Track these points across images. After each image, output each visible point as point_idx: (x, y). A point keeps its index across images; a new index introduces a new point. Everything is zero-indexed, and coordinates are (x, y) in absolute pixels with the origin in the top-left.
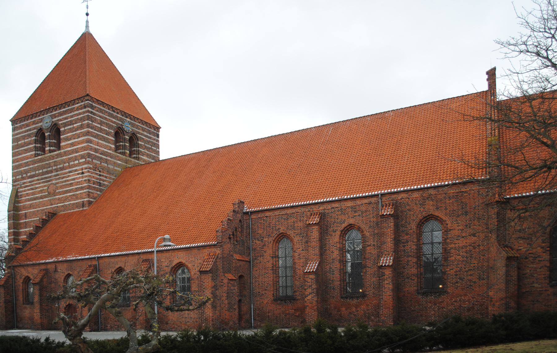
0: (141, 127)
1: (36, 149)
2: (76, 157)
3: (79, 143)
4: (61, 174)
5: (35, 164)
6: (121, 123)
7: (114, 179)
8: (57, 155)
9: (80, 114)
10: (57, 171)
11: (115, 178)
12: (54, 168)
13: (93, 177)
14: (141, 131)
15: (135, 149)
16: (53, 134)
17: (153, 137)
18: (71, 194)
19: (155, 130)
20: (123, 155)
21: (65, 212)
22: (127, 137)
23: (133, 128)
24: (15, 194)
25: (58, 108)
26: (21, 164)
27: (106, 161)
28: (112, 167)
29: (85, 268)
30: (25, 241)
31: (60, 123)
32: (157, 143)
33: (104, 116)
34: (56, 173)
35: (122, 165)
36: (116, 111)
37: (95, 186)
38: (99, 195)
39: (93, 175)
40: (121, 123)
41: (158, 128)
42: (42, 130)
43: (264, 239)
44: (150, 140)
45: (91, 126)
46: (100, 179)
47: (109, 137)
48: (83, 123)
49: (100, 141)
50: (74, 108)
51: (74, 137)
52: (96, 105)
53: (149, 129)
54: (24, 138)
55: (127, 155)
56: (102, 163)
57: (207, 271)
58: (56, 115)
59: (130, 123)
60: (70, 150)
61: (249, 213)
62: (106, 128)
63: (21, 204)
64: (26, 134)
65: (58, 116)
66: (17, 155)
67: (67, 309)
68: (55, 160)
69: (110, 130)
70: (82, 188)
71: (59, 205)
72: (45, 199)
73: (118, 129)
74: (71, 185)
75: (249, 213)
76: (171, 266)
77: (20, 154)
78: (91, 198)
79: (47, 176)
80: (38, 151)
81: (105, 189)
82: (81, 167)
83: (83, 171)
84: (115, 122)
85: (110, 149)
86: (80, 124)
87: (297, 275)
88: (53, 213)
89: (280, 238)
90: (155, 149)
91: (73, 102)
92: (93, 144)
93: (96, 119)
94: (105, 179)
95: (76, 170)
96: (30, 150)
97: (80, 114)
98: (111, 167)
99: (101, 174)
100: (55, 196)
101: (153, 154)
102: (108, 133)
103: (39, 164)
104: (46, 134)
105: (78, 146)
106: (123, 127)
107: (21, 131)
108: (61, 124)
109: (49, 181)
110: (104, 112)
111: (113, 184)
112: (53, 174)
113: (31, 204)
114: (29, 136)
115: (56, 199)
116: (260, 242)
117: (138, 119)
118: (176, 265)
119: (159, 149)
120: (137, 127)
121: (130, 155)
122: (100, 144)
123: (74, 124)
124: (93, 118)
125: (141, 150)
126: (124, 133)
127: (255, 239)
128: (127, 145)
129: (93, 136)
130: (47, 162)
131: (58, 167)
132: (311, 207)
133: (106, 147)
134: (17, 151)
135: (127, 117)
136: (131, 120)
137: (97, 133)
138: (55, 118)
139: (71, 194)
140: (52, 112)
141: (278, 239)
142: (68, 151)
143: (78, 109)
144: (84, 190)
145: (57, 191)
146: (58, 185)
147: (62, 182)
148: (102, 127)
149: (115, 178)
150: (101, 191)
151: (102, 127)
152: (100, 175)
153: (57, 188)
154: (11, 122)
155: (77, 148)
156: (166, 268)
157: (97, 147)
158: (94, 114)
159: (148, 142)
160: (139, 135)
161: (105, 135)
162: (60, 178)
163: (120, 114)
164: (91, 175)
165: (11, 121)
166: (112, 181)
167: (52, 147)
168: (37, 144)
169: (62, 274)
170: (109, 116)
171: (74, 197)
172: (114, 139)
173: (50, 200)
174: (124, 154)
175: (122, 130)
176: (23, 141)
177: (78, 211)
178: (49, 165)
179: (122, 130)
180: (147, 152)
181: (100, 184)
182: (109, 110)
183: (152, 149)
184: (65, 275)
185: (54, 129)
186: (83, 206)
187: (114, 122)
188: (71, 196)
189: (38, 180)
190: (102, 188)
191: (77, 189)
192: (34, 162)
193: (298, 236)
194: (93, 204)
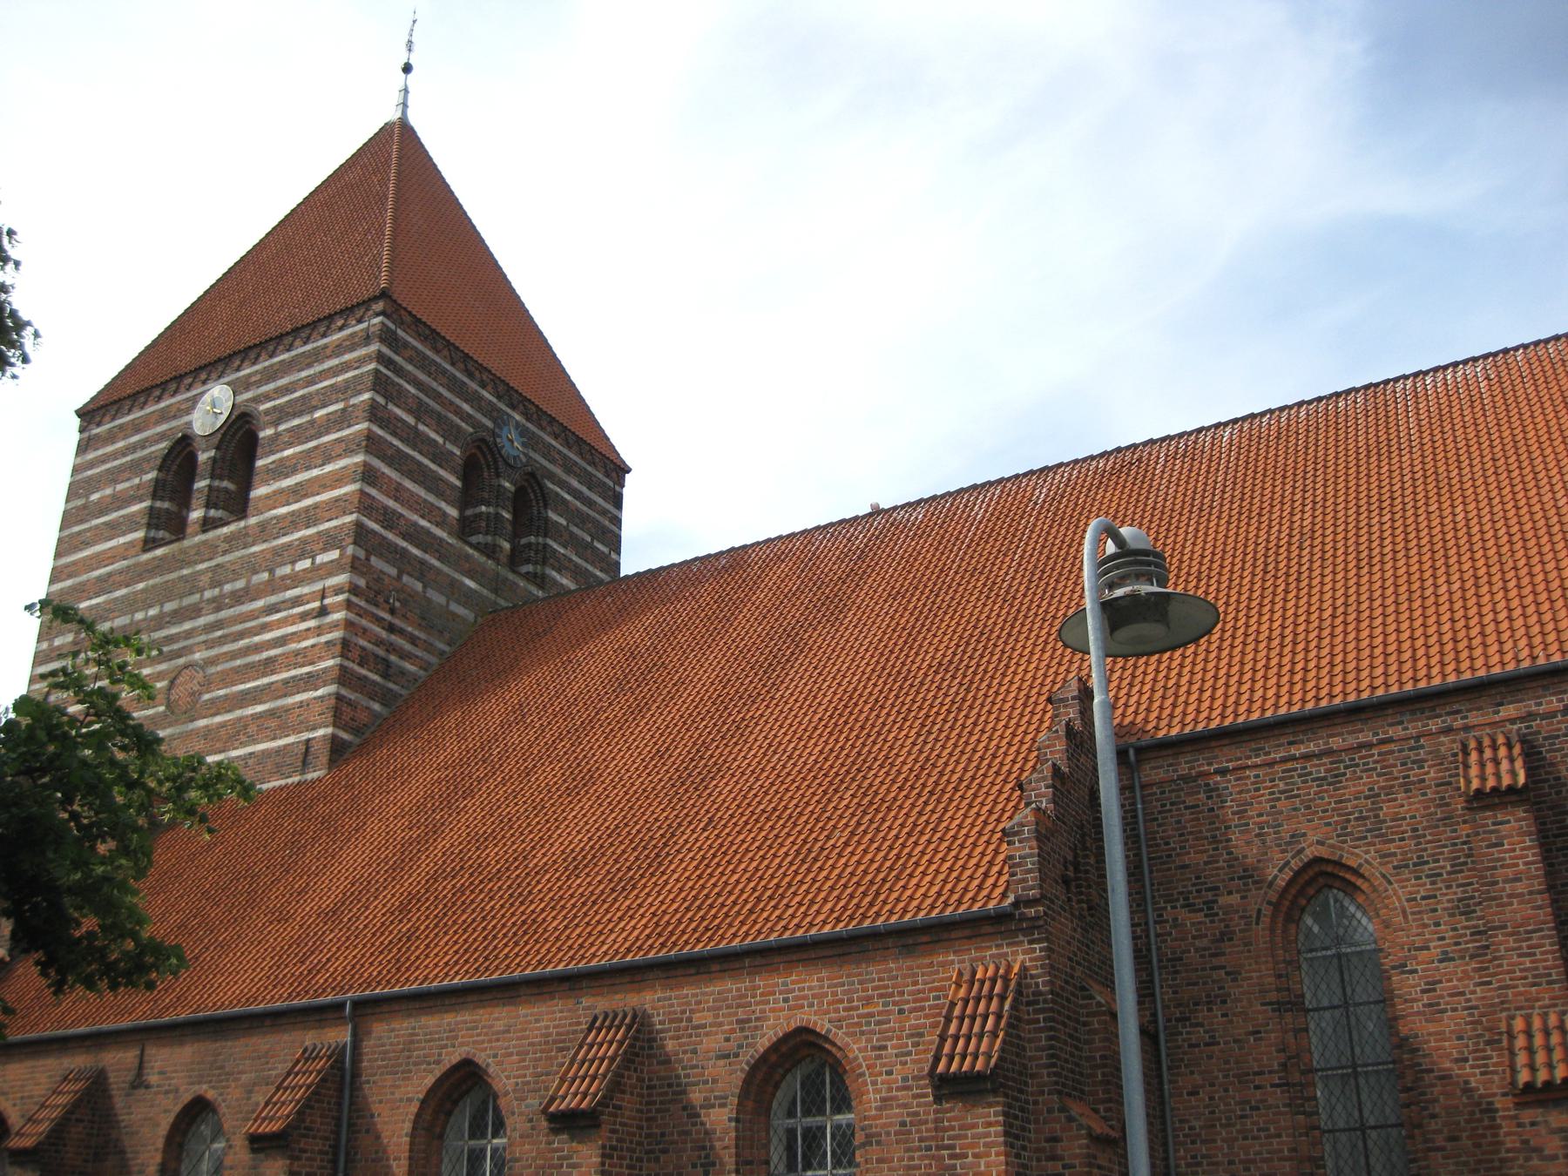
0: (559, 452)
6: (489, 424)
7: (442, 653)
8: (229, 539)
9: (346, 367)
10: (218, 609)
11: (447, 649)
12: (208, 594)
13: (365, 630)
14: (558, 471)
15: (533, 539)
17: (600, 501)
18: (260, 708)
19: (608, 476)
20: (489, 557)
22: (507, 485)
23: (532, 454)
26: (82, 584)
27: (422, 571)
28: (442, 600)
29: (281, 1068)
31: (262, 407)
32: (614, 528)
33: (434, 385)
34: (211, 618)
35: (481, 596)
36: (477, 373)
37: (364, 672)
38: (375, 715)
39: (364, 622)
40: (489, 424)
41: (620, 470)
43: (1221, 900)
44: (590, 512)
45: (379, 415)
46: (391, 648)
47: (442, 472)
48: (353, 401)
49: (408, 484)
50: (325, 347)
51: (306, 461)
52: (410, 339)
53: (589, 468)
54: (113, 477)
55: (504, 559)
56: (405, 578)
57: (980, 1077)
58: (253, 379)
59: (523, 432)
61: (1131, 752)
62: (433, 435)
65: (259, 384)
66: (77, 549)
68: (220, 560)
69: (449, 446)
73: (479, 448)
74: (269, 666)
75: (1131, 752)
76: (748, 1056)
77: (87, 544)
79: (174, 630)
80: (157, 528)
81: (404, 692)
82: (318, 586)
84: (470, 416)
87: (1433, 1116)
89: (1301, 892)
90: (606, 550)
91: (326, 322)
92: (380, 490)
93: (401, 391)
94: (408, 647)
95: (297, 601)
96: (129, 524)
97: (346, 367)
98: (438, 598)
99: (397, 622)
100: (192, 721)
101: (598, 573)
102: (440, 457)
103: (151, 582)
104: (203, 457)
105: (318, 498)
106: (498, 440)
107: (109, 449)
108: (267, 412)
111: (437, 672)
112: (201, 621)
114: (136, 468)
115: (196, 732)
116: (1200, 917)
117: (552, 420)
119: (619, 554)
120: (547, 452)
121: (514, 561)
122: (406, 495)
123: (316, 408)
124: (394, 384)
125: (555, 546)
127: (1170, 899)
128: (507, 515)
130: (185, 572)
131: (228, 588)
132: (1456, 707)
133: (428, 511)
134: (79, 533)
135: (513, 407)
136: (527, 419)
138: (247, 389)
139: (260, 708)
140: (238, 369)
141: (1295, 897)
143: (339, 349)
145: (206, 697)
146: (212, 670)
147: (234, 655)
148: (421, 427)
149: (447, 649)
150: (386, 698)
151: (421, 427)
152: (391, 629)
153: (208, 684)
154: (78, 421)
155: (316, 506)
156: (718, 1068)
157: (391, 503)
161: (426, 462)
163: (489, 387)
165: (81, 413)
166: (434, 660)
167: (216, 507)
170: (449, 389)
171: (273, 724)
172: (458, 483)
174: (490, 551)
176: (108, 491)
177: (281, 788)
178: (191, 584)
179: (490, 450)
180: (574, 558)
181: (386, 670)
182: (453, 364)
184: (178, 1108)
185: (235, 434)
187: (467, 418)
190: (391, 685)
193: (1406, 874)
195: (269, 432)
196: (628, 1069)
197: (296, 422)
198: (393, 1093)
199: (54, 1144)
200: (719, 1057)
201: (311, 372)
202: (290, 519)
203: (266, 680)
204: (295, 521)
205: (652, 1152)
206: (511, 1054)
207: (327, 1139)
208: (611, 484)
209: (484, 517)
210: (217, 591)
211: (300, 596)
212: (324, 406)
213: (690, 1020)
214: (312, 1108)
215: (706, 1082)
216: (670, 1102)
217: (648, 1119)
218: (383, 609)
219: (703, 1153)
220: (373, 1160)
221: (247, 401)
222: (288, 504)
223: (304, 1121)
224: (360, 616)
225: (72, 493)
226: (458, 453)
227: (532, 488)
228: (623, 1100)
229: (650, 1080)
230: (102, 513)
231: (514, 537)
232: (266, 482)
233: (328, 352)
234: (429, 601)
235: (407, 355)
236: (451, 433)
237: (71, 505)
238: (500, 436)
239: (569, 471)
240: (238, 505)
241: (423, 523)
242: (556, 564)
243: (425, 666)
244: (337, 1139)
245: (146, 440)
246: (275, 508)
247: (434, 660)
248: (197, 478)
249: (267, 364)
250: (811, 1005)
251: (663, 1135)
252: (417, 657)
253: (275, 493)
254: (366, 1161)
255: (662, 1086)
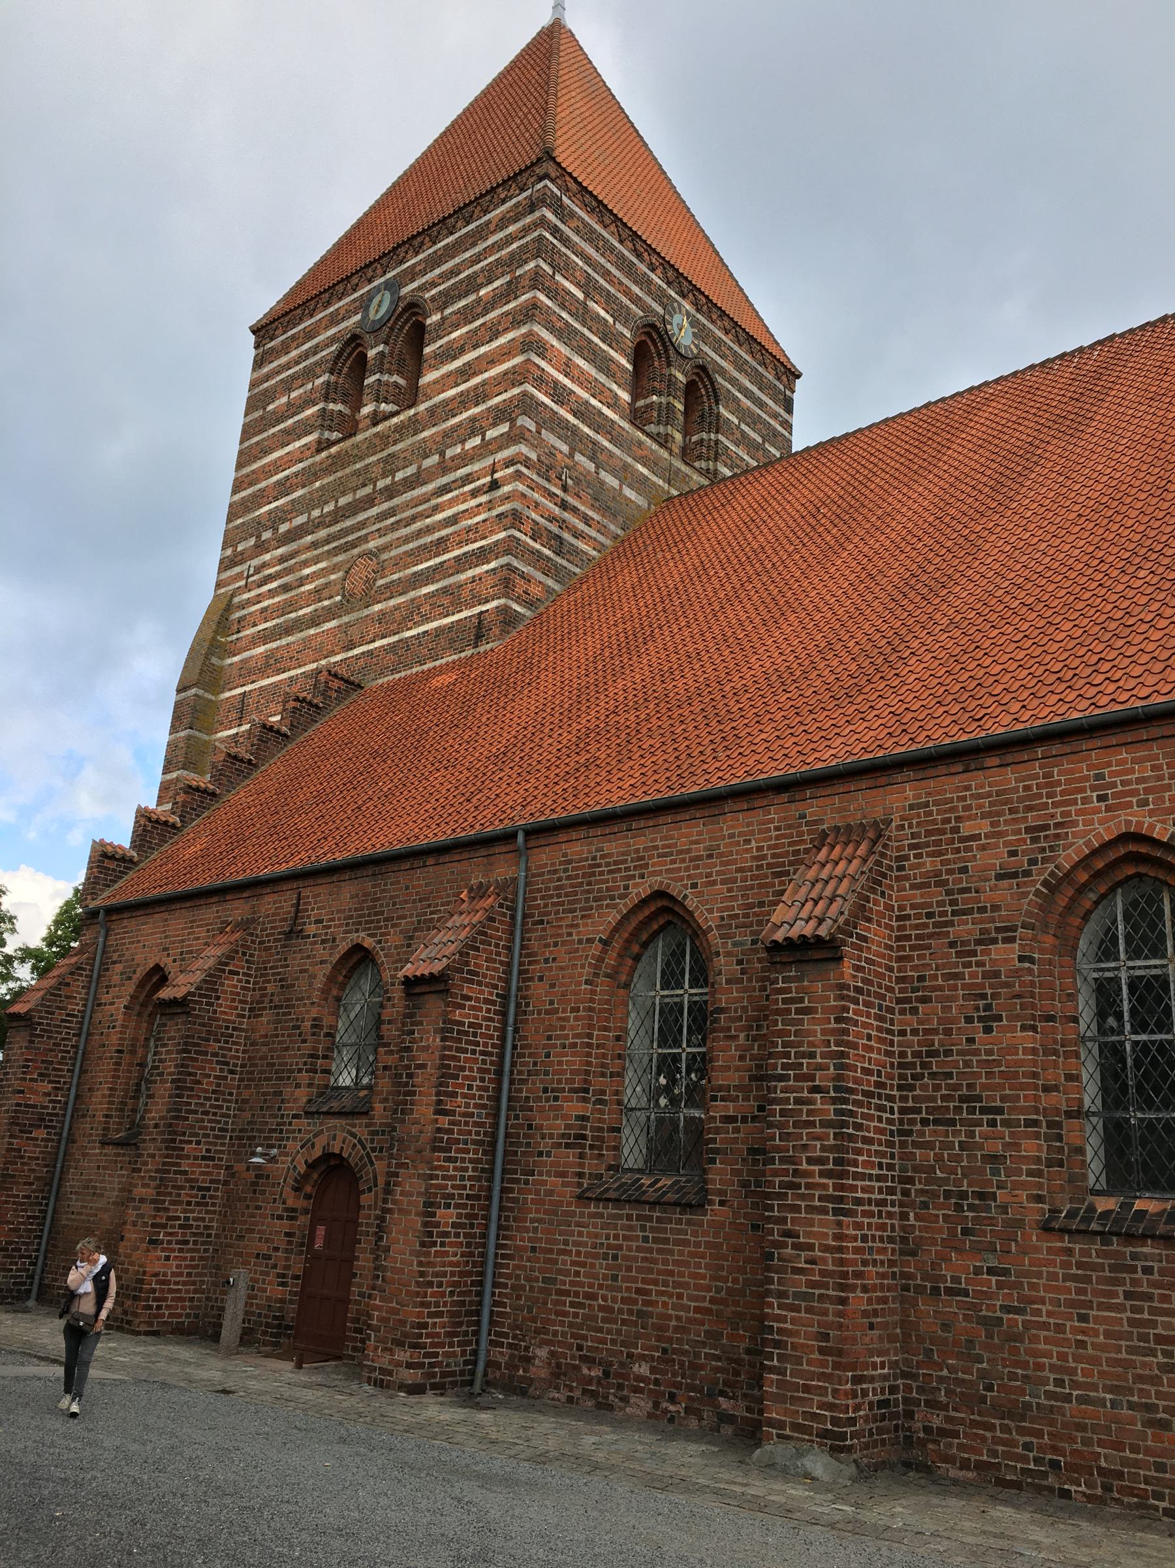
0: (730, 348)
1: (325, 420)
2: (473, 419)
3: (491, 360)
4: (407, 505)
5: (313, 482)
6: (660, 310)
7: (616, 537)
10: (391, 498)
11: (619, 532)
12: (381, 484)
13: (537, 505)
15: (704, 435)
16: (396, 351)
17: (770, 403)
18: (431, 588)
19: (779, 379)
20: (661, 445)
21: (397, 676)
24: (216, 618)
25: (427, 239)
26: (263, 490)
27: (594, 450)
30: (197, 789)
34: (385, 506)
38: (549, 591)
40: (660, 310)
42: (359, 345)
44: (760, 412)
46: (563, 524)
47: (612, 353)
50: (489, 222)
52: (577, 209)
53: (760, 369)
58: (418, 269)
59: (694, 323)
60: (453, 398)
62: (603, 313)
63: (236, 659)
64: (297, 368)
67: (308, 1189)
70: (482, 556)
71: (377, 644)
72: (327, 626)
73: (648, 334)
74: (441, 545)
76: (1041, 875)
77: (266, 452)
78: (518, 600)
79: (348, 523)
82: (488, 461)
83: (496, 476)
85: (614, 404)
86: (507, 278)
88: (347, 681)
91: (489, 197)
92: (550, 362)
94: (581, 526)
95: (467, 479)
98: (611, 481)
99: (569, 499)
103: (325, 481)
105: (486, 375)
106: (669, 327)
107: (284, 360)
108: (433, 299)
109: (353, 545)
110: (601, 243)
112: (374, 511)
113: (268, 656)
114: (309, 374)
117: (723, 314)
118: (1084, 863)
121: (687, 454)
122: (576, 372)
123: (481, 286)
124: (561, 254)
126: (668, 358)
129: (552, 329)
130: (358, 466)
131: (399, 476)
133: (597, 390)
134: (257, 443)
135: (684, 296)
136: (698, 310)
137: (570, 320)
139: (431, 588)
142: (445, 403)
143: (503, 223)
144: (488, 562)
146: (384, 556)
147: (407, 540)
149: (619, 532)
152: (564, 505)
153: (381, 571)
155: (484, 383)
156: (1004, 893)
158: (565, 241)
159: (754, 422)
160: (720, 380)
161: (596, 340)
162: (397, 522)
163: (659, 271)
164: (529, 492)
165: (255, 330)
166: (608, 542)
168: (334, 401)
169: (320, 952)
172: (630, 367)
173: (348, 625)
174: (663, 441)
175: (662, 340)
179: (660, 336)
181: (559, 545)
182: (621, 242)
183: (765, 450)
185: (402, 327)
186: (479, 638)
187: (636, 300)
188: (432, 595)
189: (315, 545)
191: (462, 563)
192: (311, 475)
194: (521, 627)
195: (436, 318)
196: (874, 891)
197: (463, 303)
198: (570, 934)
199: (205, 996)
200: (999, 877)
201: (477, 249)
202: (459, 400)
203: (438, 560)
204: (464, 401)
205: (908, 1000)
206: (714, 883)
207: (495, 987)
208: (782, 387)
209: (656, 407)
210: (388, 481)
211: (471, 474)
212: (490, 282)
213: (956, 830)
214: (477, 949)
215: (983, 910)
216: (931, 936)
217: (899, 959)
218: (555, 485)
219: (981, 1003)
220: (547, 1012)
221: (412, 291)
222: (457, 385)
223: (467, 964)
224: (533, 490)
225: (251, 406)
226: (628, 335)
227: (703, 383)
228: (868, 929)
229: (901, 908)
230: (279, 421)
231: (686, 433)
232: (435, 368)
233: (492, 227)
234: (602, 483)
235: (572, 226)
236: (620, 313)
237: (249, 418)
238: (671, 324)
239: (740, 370)
240: (410, 395)
241: (593, 402)
242: (729, 462)
243: (600, 547)
244: (508, 988)
245: (317, 346)
246: (443, 391)
247: (608, 542)
248: (368, 374)
249: (431, 251)
250: (1143, 803)
251: (921, 979)
252: (591, 537)
253: (443, 377)
254: (539, 1013)
255: (918, 916)
